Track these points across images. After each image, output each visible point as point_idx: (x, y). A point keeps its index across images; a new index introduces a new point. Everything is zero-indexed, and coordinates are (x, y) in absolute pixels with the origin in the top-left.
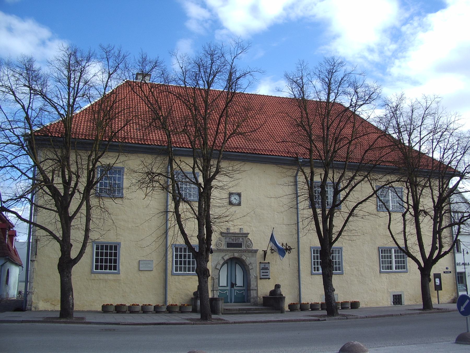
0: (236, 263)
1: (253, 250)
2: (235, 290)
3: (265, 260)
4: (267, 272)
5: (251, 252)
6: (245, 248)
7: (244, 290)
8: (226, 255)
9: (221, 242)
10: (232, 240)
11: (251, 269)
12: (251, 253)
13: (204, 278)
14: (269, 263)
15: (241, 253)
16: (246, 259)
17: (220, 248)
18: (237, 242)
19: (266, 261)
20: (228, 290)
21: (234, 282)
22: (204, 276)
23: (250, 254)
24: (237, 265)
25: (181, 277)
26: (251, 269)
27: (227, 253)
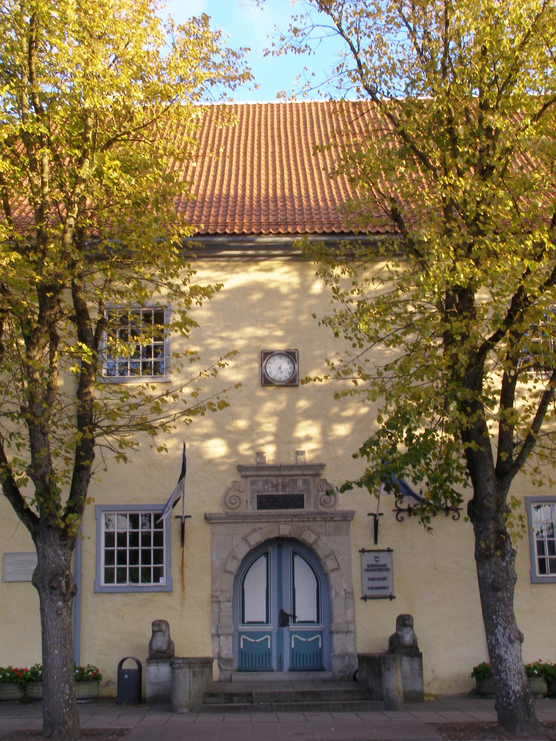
0: (294, 554)
1: (336, 513)
2: (292, 633)
3: (376, 542)
4: (385, 579)
5: (332, 519)
6: (312, 509)
7: (321, 633)
8: (255, 530)
9: (238, 494)
10: (275, 486)
11: (333, 570)
12: (332, 524)
13: (52, 600)
14: (389, 550)
15: (301, 524)
16: (316, 541)
17: (237, 511)
18: (289, 491)
19: (380, 546)
20: (270, 633)
21: (288, 610)
22: (51, 593)
23: (330, 525)
24: (298, 560)
25: (119, 598)
26: (333, 570)
27: (257, 525)
